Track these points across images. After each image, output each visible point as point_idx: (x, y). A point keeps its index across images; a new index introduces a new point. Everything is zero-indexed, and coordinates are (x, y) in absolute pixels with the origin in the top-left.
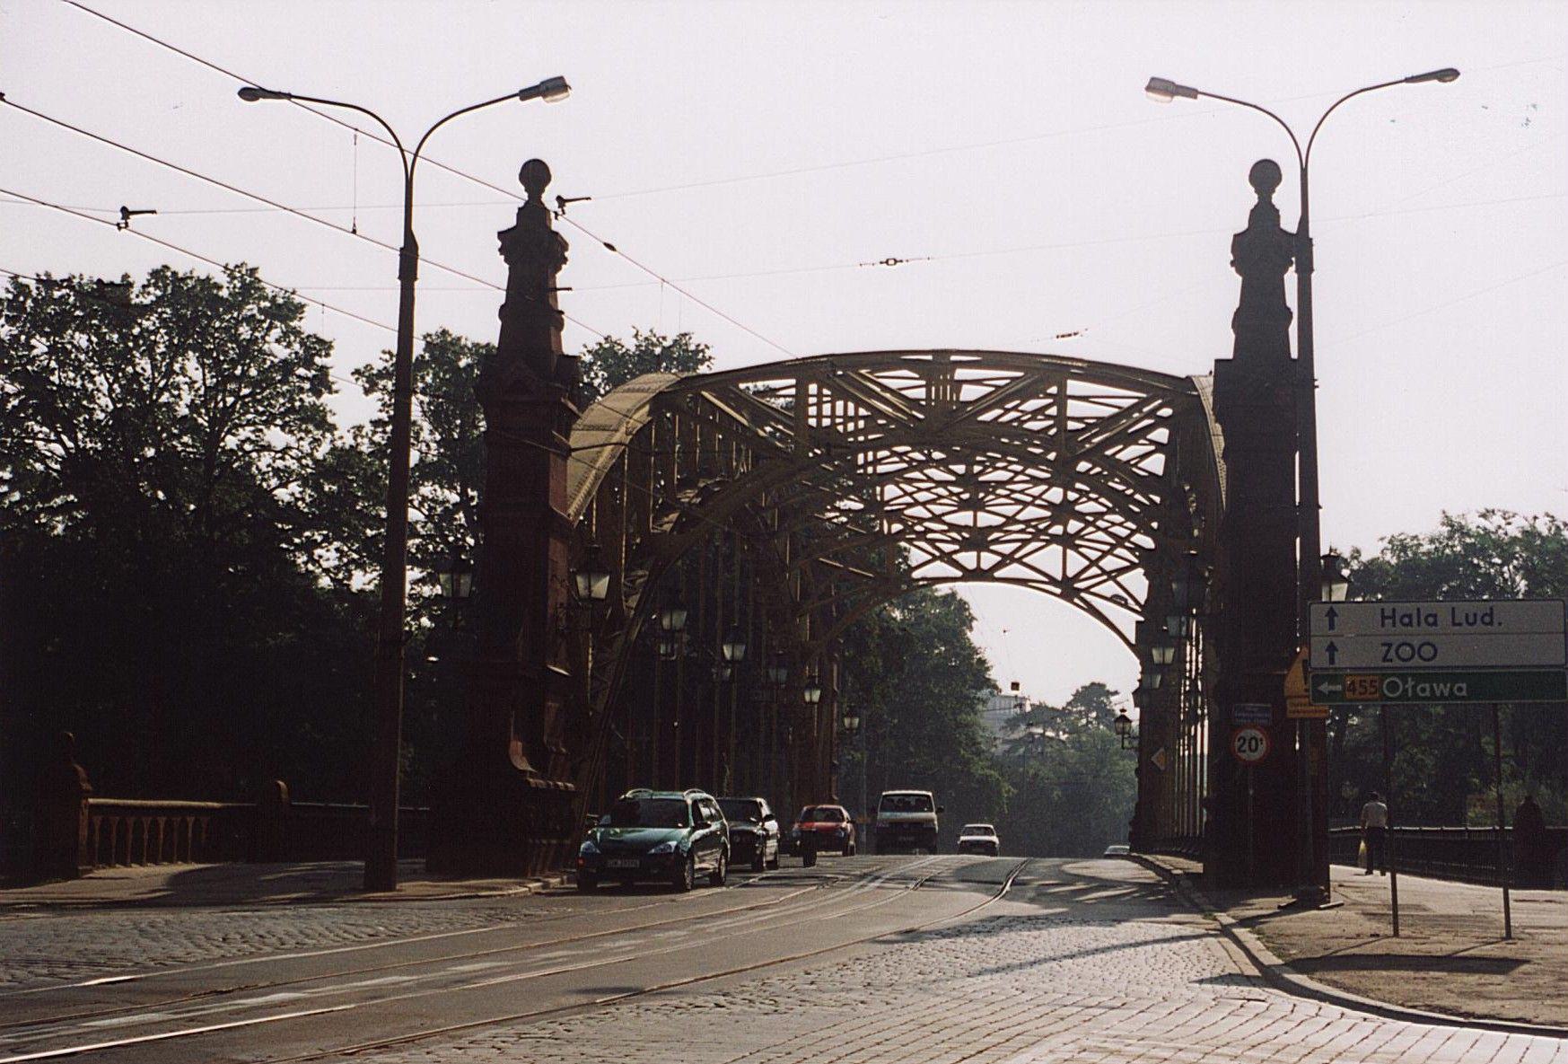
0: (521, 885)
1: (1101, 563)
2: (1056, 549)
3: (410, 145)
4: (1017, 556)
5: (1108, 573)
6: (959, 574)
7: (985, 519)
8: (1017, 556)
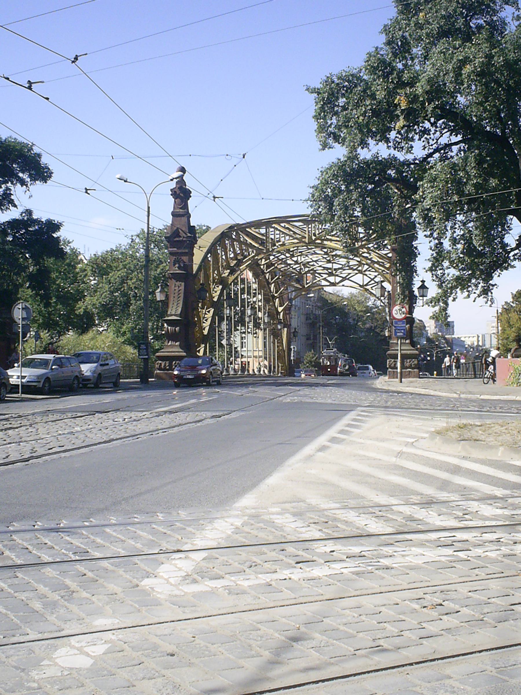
0: (194, 396)
1: (375, 280)
2: (360, 275)
3: (148, 191)
4: (347, 277)
5: (377, 282)
6: (328, 284)
7: (336, 266)
8: (347, 277)
